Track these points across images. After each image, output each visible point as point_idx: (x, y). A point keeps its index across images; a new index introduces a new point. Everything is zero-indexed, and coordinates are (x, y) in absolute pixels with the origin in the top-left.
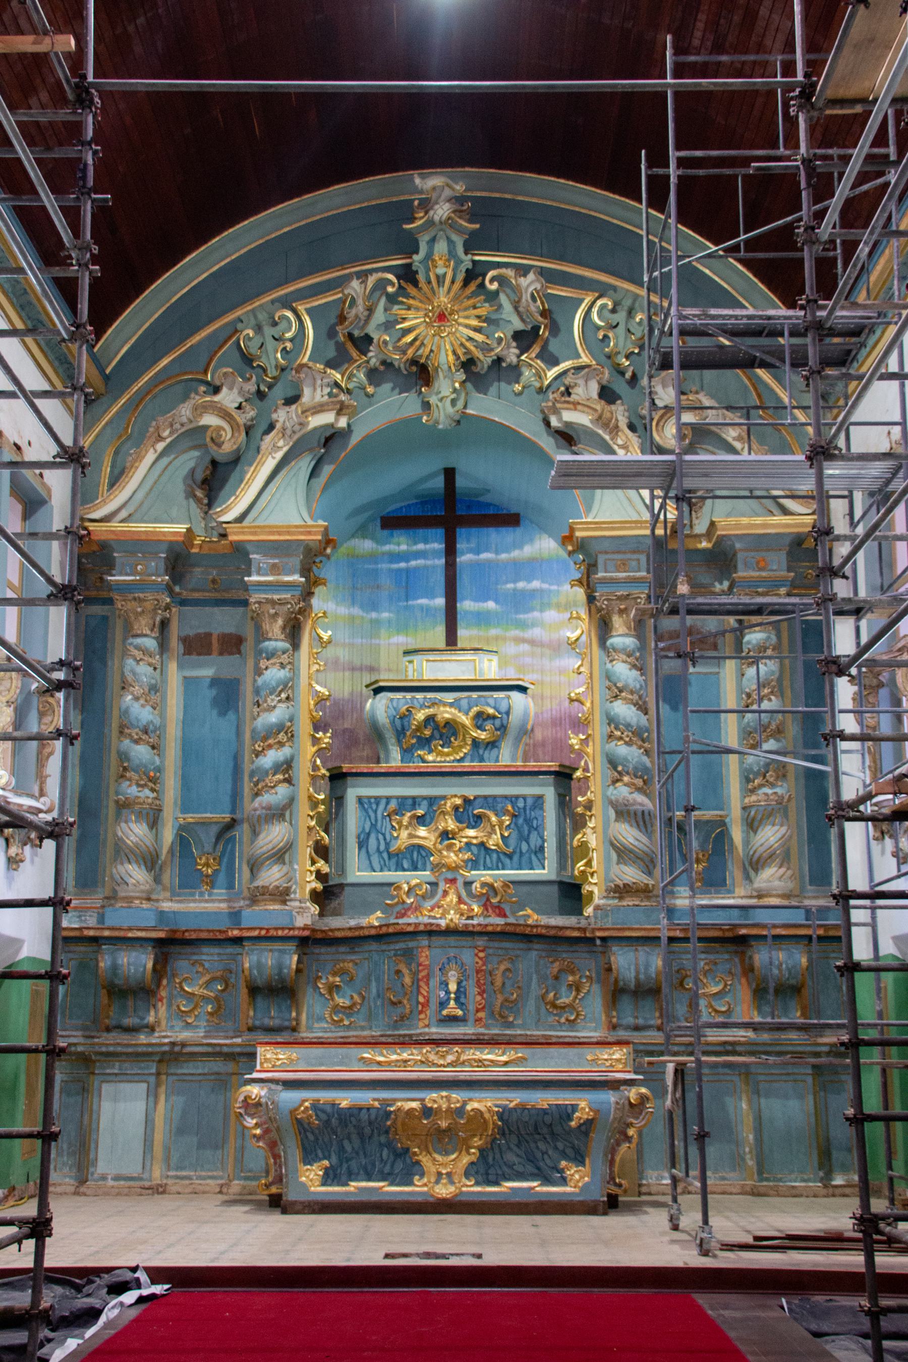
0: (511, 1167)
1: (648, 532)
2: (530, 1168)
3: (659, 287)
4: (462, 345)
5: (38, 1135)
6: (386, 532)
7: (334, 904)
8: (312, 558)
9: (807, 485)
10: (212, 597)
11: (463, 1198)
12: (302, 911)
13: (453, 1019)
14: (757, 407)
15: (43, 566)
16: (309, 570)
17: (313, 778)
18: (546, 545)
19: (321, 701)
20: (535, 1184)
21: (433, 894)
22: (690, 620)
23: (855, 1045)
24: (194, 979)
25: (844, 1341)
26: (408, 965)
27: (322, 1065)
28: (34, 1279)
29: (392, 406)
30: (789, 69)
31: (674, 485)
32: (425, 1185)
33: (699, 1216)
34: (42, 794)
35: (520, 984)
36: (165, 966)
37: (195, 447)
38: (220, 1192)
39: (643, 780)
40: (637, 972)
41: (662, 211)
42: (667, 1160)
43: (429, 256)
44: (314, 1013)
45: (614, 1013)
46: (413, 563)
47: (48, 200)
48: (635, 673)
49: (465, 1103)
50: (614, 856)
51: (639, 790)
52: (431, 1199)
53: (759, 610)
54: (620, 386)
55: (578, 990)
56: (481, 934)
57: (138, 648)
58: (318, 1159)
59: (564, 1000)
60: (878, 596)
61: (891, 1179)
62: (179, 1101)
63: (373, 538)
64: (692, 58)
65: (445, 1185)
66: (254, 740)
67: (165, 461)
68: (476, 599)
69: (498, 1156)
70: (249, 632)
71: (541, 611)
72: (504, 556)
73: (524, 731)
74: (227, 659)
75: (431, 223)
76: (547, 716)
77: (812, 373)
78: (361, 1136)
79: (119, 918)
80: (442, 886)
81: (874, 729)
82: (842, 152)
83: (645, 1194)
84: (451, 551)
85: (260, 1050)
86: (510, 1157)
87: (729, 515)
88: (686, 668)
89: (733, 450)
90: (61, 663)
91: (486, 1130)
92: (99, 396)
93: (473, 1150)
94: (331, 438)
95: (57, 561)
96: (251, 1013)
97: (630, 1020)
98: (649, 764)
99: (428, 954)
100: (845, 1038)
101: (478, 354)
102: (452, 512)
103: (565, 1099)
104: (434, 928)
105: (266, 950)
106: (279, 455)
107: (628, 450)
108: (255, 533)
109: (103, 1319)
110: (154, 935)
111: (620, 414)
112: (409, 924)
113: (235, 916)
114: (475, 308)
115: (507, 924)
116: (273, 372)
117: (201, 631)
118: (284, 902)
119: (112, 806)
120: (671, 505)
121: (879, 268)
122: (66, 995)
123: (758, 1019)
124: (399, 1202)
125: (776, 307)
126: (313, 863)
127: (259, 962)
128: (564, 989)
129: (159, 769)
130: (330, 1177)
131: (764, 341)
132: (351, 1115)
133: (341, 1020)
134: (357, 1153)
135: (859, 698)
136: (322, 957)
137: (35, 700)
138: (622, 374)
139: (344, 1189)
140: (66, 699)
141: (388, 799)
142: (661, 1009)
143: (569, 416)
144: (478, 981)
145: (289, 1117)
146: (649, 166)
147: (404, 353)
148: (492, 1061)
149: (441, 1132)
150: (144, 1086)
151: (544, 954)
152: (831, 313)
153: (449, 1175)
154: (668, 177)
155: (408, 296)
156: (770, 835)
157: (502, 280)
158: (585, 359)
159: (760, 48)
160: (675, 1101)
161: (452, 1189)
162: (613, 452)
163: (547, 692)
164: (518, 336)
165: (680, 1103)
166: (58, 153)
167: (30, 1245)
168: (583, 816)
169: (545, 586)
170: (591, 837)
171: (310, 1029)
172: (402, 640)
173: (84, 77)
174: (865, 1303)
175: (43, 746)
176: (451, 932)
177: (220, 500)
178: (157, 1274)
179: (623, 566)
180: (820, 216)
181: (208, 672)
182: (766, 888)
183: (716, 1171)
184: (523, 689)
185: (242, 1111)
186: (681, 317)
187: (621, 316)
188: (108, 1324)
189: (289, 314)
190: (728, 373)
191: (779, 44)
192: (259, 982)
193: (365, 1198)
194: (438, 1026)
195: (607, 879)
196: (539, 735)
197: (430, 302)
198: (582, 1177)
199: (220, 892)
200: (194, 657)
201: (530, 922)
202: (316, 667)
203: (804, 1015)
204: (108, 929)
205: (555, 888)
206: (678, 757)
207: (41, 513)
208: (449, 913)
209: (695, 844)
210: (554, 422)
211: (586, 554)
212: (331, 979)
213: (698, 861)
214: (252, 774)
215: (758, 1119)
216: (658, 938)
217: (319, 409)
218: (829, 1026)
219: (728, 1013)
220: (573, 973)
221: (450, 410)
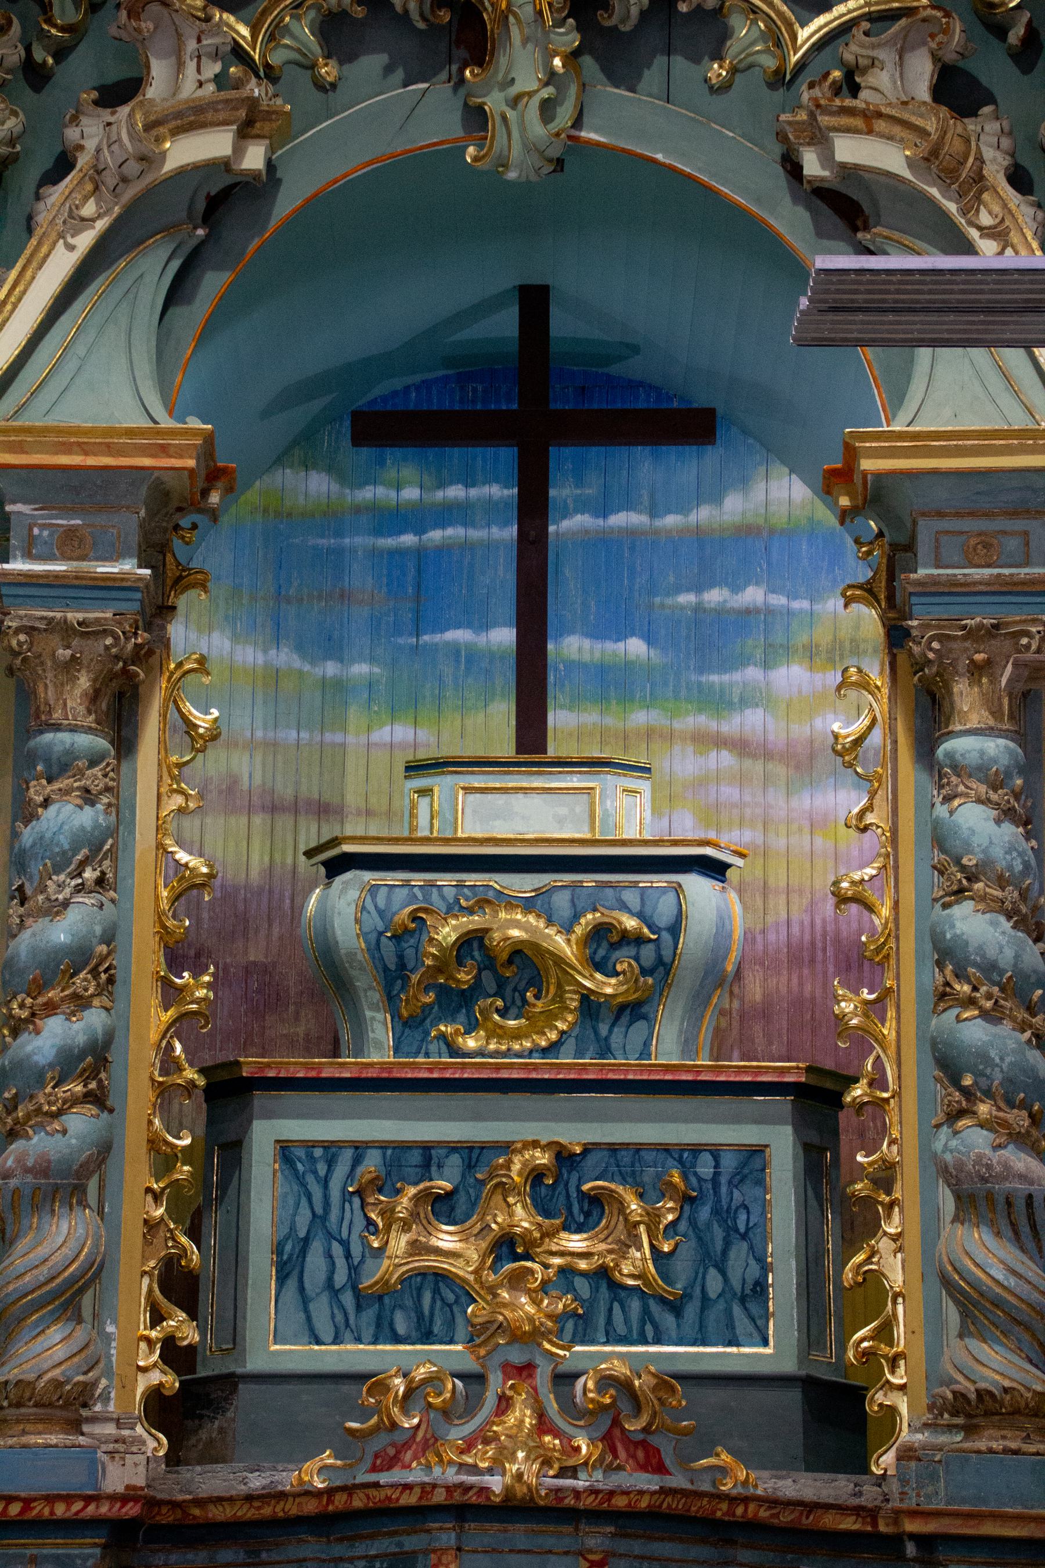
7: (209, 1430)
8: (170, 515)
12: (121, 1449)
17: (163, 1091)
18: (784, 494)
19: (188, 888)
46: (436, 535)
48: (1010, 831)
50: (952, 1314)
51: (1019, 1139)
54: (994, 70)
56: (595, 1516)
63: (331, 468)
68: (597, 634)
71: (767, 665)
72: (671, 520)
73: (717, 978)
76: (776, 938)
80: (496, 1383)
84: (533, 509)
94: (224, 200)
102: (541, 405)
104: (472, 1498)
106: (85, 241)
111: (989, 142)
112: (407, 1487)
115: (664, 1491)
118: (75, 1426)
126: (157, 1318)
138: (1000, 31)
141: (360, 1148)
143: (850, 149)
162: (969, 249)
163: (778, 878)
168: (869, 1202)
169: (778, 600)
172: (401, 734)
176: (517, 1509)
184: (715, 869)
195: (934, 1377)
196: (755, 988)
202: (179, 800)
205: (794, 1397)
208: (513, 1459)
210: (812, 165)
217: (191, 119)
221: (538, 130)
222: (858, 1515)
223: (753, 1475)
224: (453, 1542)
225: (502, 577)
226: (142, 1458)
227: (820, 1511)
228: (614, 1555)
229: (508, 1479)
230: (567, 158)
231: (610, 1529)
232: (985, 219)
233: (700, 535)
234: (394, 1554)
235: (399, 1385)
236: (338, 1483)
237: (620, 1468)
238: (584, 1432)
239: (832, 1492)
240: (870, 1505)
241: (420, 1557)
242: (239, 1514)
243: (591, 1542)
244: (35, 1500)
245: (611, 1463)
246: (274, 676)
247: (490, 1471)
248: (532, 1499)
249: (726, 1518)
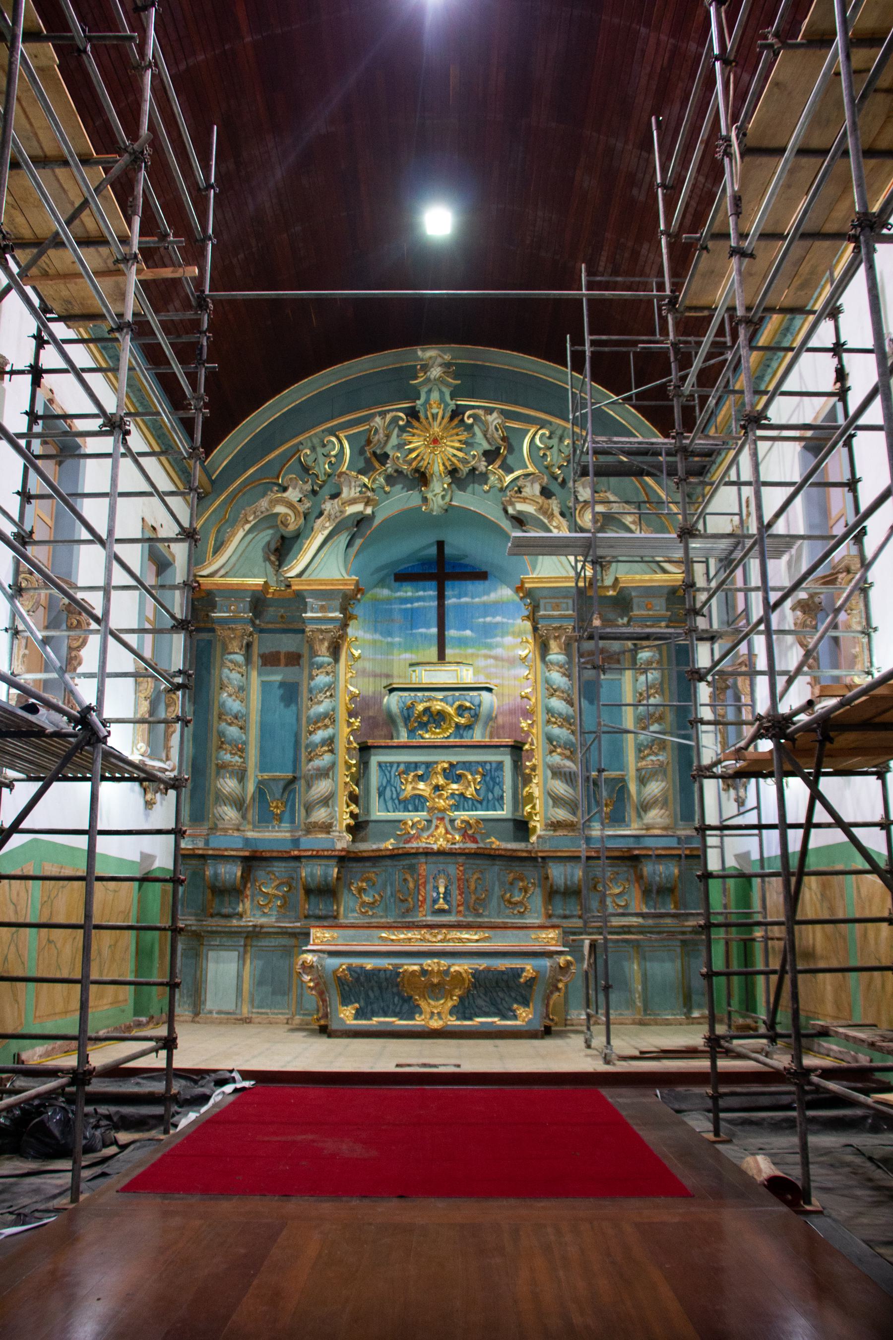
0: (480, 1008)
1: (573, 584)
2: (493, 1009)
3: (579, 422)
4: (449, 459)
5: (167, 984)
6: (397, 584)
7: (362, 834)
8: (347, 602)
9: (679, 554)
10: (281, 628)
11: (448, 1029)
12: (340, 838)
13: (441, 911)
14: (645, 502)
15: (168, 607)
16: (346, 609)
17: (348, 749)
18: (505, 593)
19: (353, 697)
21: (428, 828)
22: (602, 643)
23: (708, 927)
24: (269, 884)
25: (695, 1115)
28: (167, 1075)
29: (402, 499)
30: (661, 287)
31: (591, 553)
33: (604, 1039)
34: (168, 759)
36: (249, 875)
37: (269, 528)
39: (570, 751)
40: (566, 879)
41: (581, 374)
42: (584, 1002)
43: (427, 401)
44: (349, 907)
46: (416, 605)
47: (177, 368)
48: (565, 679)
49: (449, 967)
50: (551, 802)
51: (568, 758)
53: (647, 637)
54: (555, 487)
55: (526, 892)
56: (460, 854)
57: (231, 661)
58: (351, 1003)
59: (516, 899)
60: (725, 628)
61: (729, 1013)
62: (259, 963)
63: (389, 588)
64: (598, 279)
66: (308, 723)
67: (250, 536)
68: (458, 629)
70: (305, 651)
71: (502, 637)
72: (477, 600)
73: (490, 718)
74: (290, 669)
75: (428, 380)
76: (506, 707)
77: (681, 480)
78: (380, 988)
79: (219, 842)
80: (435, 822)
81: (723, 716)
82: (697, 339)
84: (441, 597)
85: (313, 931)
86: (480, 1002)
87: (627, 573)
88: (599, 676)
89: (630, 530)
90: (180, 672)
92: (207, 494)
94: (361, 521)
95: (178, 603)
97: (561, 912)
98: (574, 740)
99: (424, 868)
100: (702, 922)
101: (460, 465)
102: (442, 571)
106: (326, 532)
107: (560, 530)
108: (309, 585)
109: (212, 1102)
110: (241, 854)
111: (554, 505)
113: (296, 842)
114: (457, 435)
116: (322, 477)
117: (274, 650)
118: (328, 833)
119: (214, 767)
120: (589, 566)
121: (723, 413)
122: (184, 892)
123: (645, 910)
125: (657, 437)
126: (348, 806)
128: (516, 892)
129: (244, 743)
130: (359, 1014)
131: (649, 459)
135: (713, 696)
137: (163, 696)
138: (556, 479)
140: (183, 696)
141: (399, 764)
142: (581, 905)
143: (520, 507)
146: (572, 345)
147: (410, 464)
149: (433, 985)
150: (236, 953)
152: (692, 441)
153: (439, 1013)
154: (584, 352)
155: (413, 427)
156: (655, 788)
157: (475, 417)
158: (531, 469)
159: (642, 274)
160: (589, 965)
161: (441, 1023)
162: (550, 531)
163: (506, 691)
164: (486, 453)
166: (185, 339)
167: (163, 1053)
168: (530, 775)
169: (505, 620)
170: (535, 789)
171: (346, 917)
172: (408, 656)
173: (203, 291)
174: (710, 1091)
175: (169, 727)
176: (441, 853)
177: (287, 562)
178: (246, 1075)
179: (557, 607)
180: (683, 379)
181: (278, 678)
182: (651, 824)
183: (616, 1010)
184: (489, 690)
186: (594, 442)
187: (554, 441)
188: (215, 1105)
189: (334, 439)
190: (626, 479)
191: (654, 271)
192: (312, 886)
193: (383, 1028)
195: (546, 818)
196: (500, 720)
197: (428, 431)
199: (286, 825)
200: (269, 668)
201: (494, 846)
202: (350, 675)
203: (676, 907)
204: (213, 849)
205: (511, 824)
206: (594, 735)
207: (169, 571)
209: (604, 794)
210: (511, 510)
211: (533, 599)
213: (607, 805)
214: (307, 746)
215: (645, 975)
216: (579, 857)
217: (353, 502)
218: (692, 914)
219: (626, 906)
220: (522, 880)
221: (441, 502)
225: (433, 616)
230: (449, 509)
232: (554, 524)
233: (485, 605)
235: (410, 823)
246: (375, 642)
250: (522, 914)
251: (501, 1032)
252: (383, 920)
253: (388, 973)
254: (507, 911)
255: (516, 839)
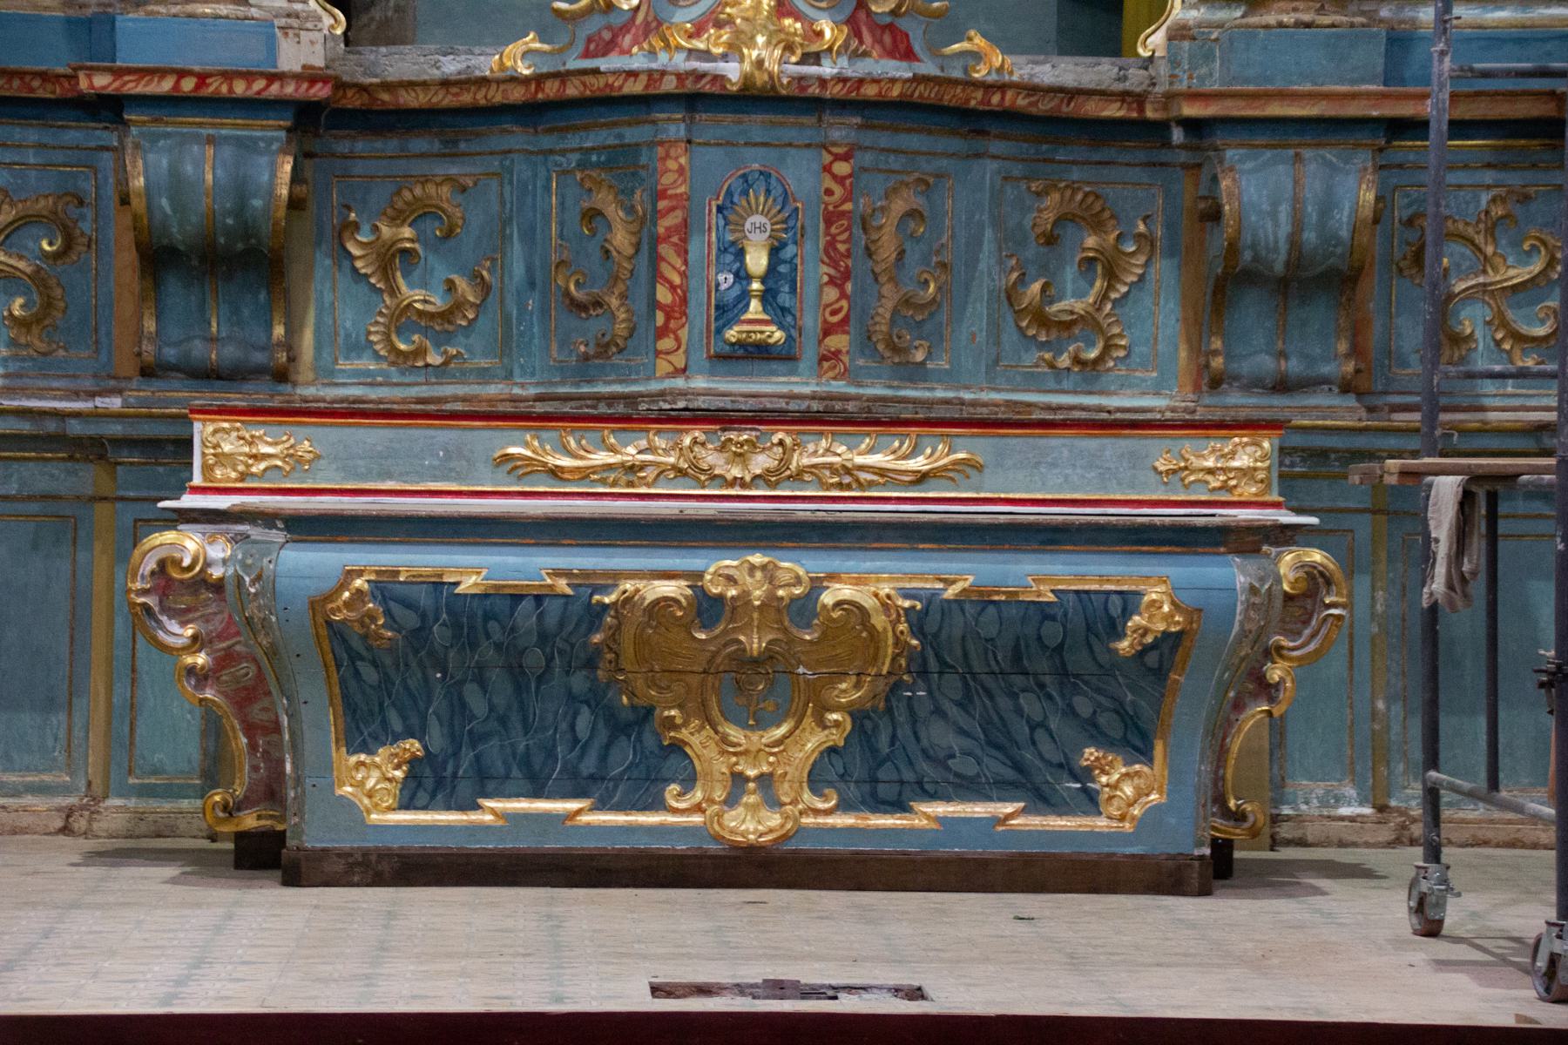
0: (941, 762)
2: (996, 767)
13: (755, 354)
20: (1009, 808)
26: (624, 195)
27: (389, 476)
32: (698, 808)
35: (946, 257)
38: (66, 830)
40: (1298, 224)
44: (336, 329)
45: (1217, 344)
49: (817, 586)
52: (712, 847)
55: (1112, 276)
56: (841, 106)
58: (387, 736)
59: (1070, 304)
65: (753, 808)
69: (904, 732)
78: (517, 673)
83: (1289, 843)
85: (202, 430)
86: (940, 736)
91: (875, 659)
93: (835, 716)
96: (150, 325)
97: (1265, 363)
99: (681, 162)
103: (1102, 579)
104: (705, 86)
105: (196, 138)
112: (633, 74)
115: (918, 79)
124: (619, 855)
127: (175, 173)
128: (1070, 273)
130: (422, 785)
132: (487, 617)
133: (420, 352)
134: (503, 721)
136: (359, 168)
139: (473, 817)
144: (831, 244)
145: (308, 622)
148: (881, 471)
151: (1017, 170)
153: (765, 781)
160: (1458, 581)
161: (774, 820)
165: (1479, 588)
171: (326, 374)
176: (756, 99)
185: (151, 601)
192: (177, 234)
194: (712, 373)
198: (1140, 793)
208: (751, 43)
212: (386, 231)
220: (1097, 225)
222: (1123, 101)
223: (1009, 60)
224: (682, 133)
226: (318, 36)
227: (1081, 99)
228: (860, 148)
229: (747, 67)
231: (857, 120)
234: (615, 147)
236: (545, 70)
237: (866, 54)
238: (826, 14)
239: (1095, 78)
240: (1138, 90)
241: (644, 151)
242: (435, 100)
243: (836, 134)
244: (210, 75)
245: (857, 49)
247: (724, 57)
248: (773, 87)
249: (981, 108)
250: (1089, 370)
251: (1028, 860)
252: (493, 390)
253: (553, 609)
254: (1031, 357)
255: (1074, 43)
